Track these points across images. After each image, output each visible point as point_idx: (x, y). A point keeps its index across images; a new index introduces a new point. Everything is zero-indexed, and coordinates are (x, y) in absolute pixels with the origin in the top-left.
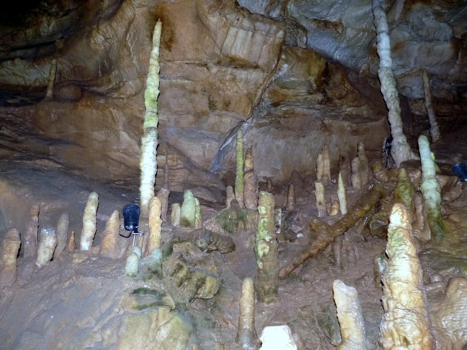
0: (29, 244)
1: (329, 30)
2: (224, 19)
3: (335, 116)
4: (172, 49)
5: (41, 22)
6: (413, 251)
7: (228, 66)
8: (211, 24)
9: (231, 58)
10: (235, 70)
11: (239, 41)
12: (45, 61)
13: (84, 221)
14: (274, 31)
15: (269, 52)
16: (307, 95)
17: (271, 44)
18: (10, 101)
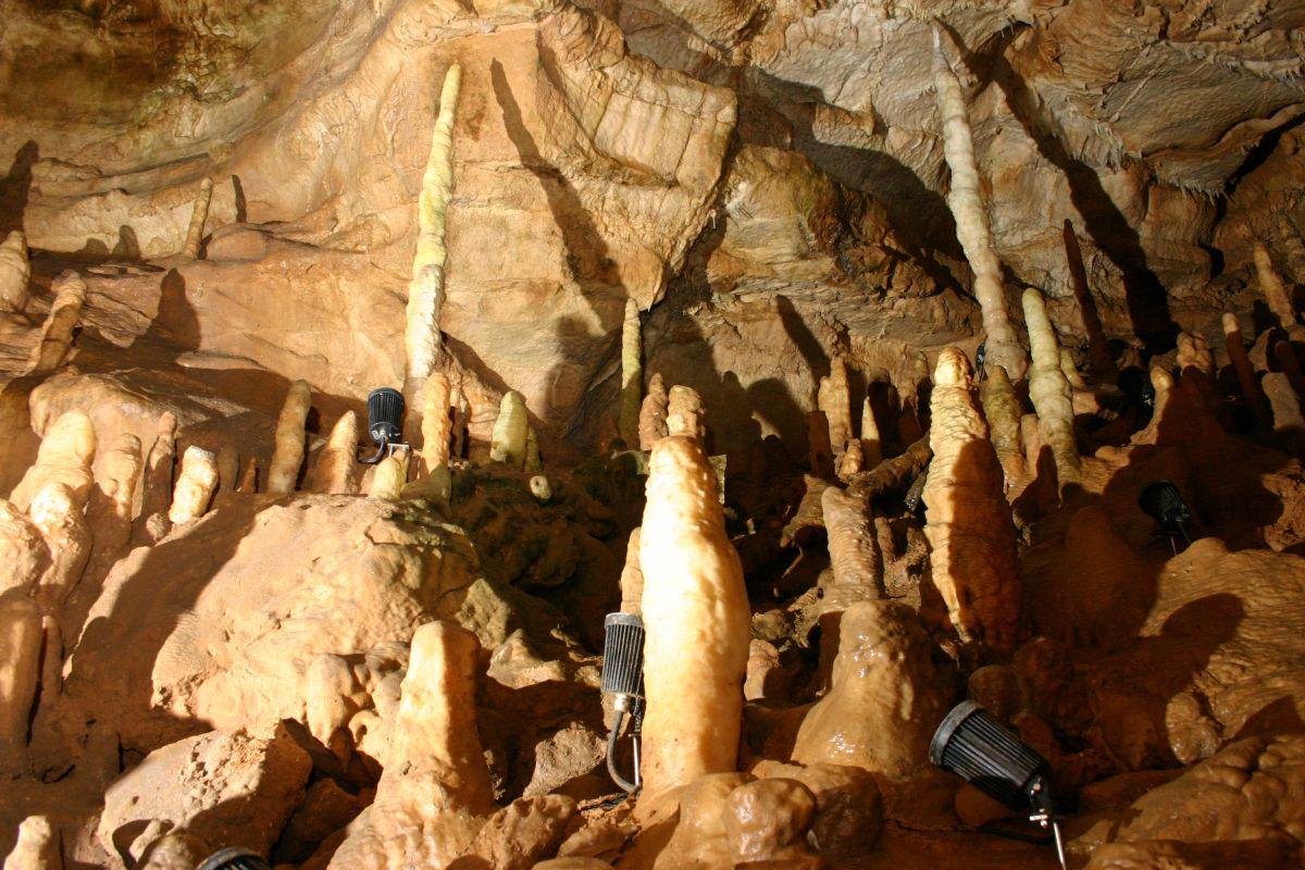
0: (154, 487)
1: (845, 128)
2: (599, 75)
3: (868, 320)
4: (481, 134)
5: (178, 116)
6: (981, 429)
7: (609, 178)
8: (570, 84)
9: (614, 160)
10: (624, 189)
11: (631, 130)
12: (180, 195)
13: (278, 437)
14: (713, 106)
15: (702, 151)
16: (795, 262)
17: (705, 135)
18: (96, 271)
